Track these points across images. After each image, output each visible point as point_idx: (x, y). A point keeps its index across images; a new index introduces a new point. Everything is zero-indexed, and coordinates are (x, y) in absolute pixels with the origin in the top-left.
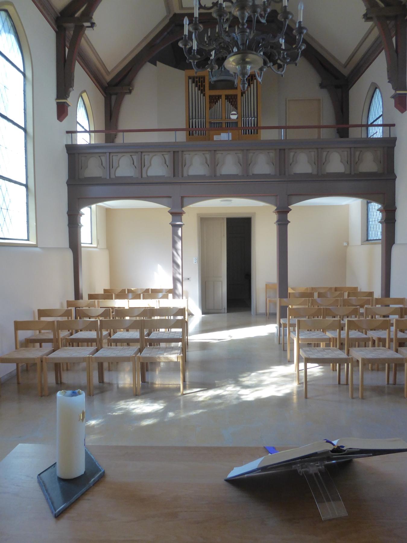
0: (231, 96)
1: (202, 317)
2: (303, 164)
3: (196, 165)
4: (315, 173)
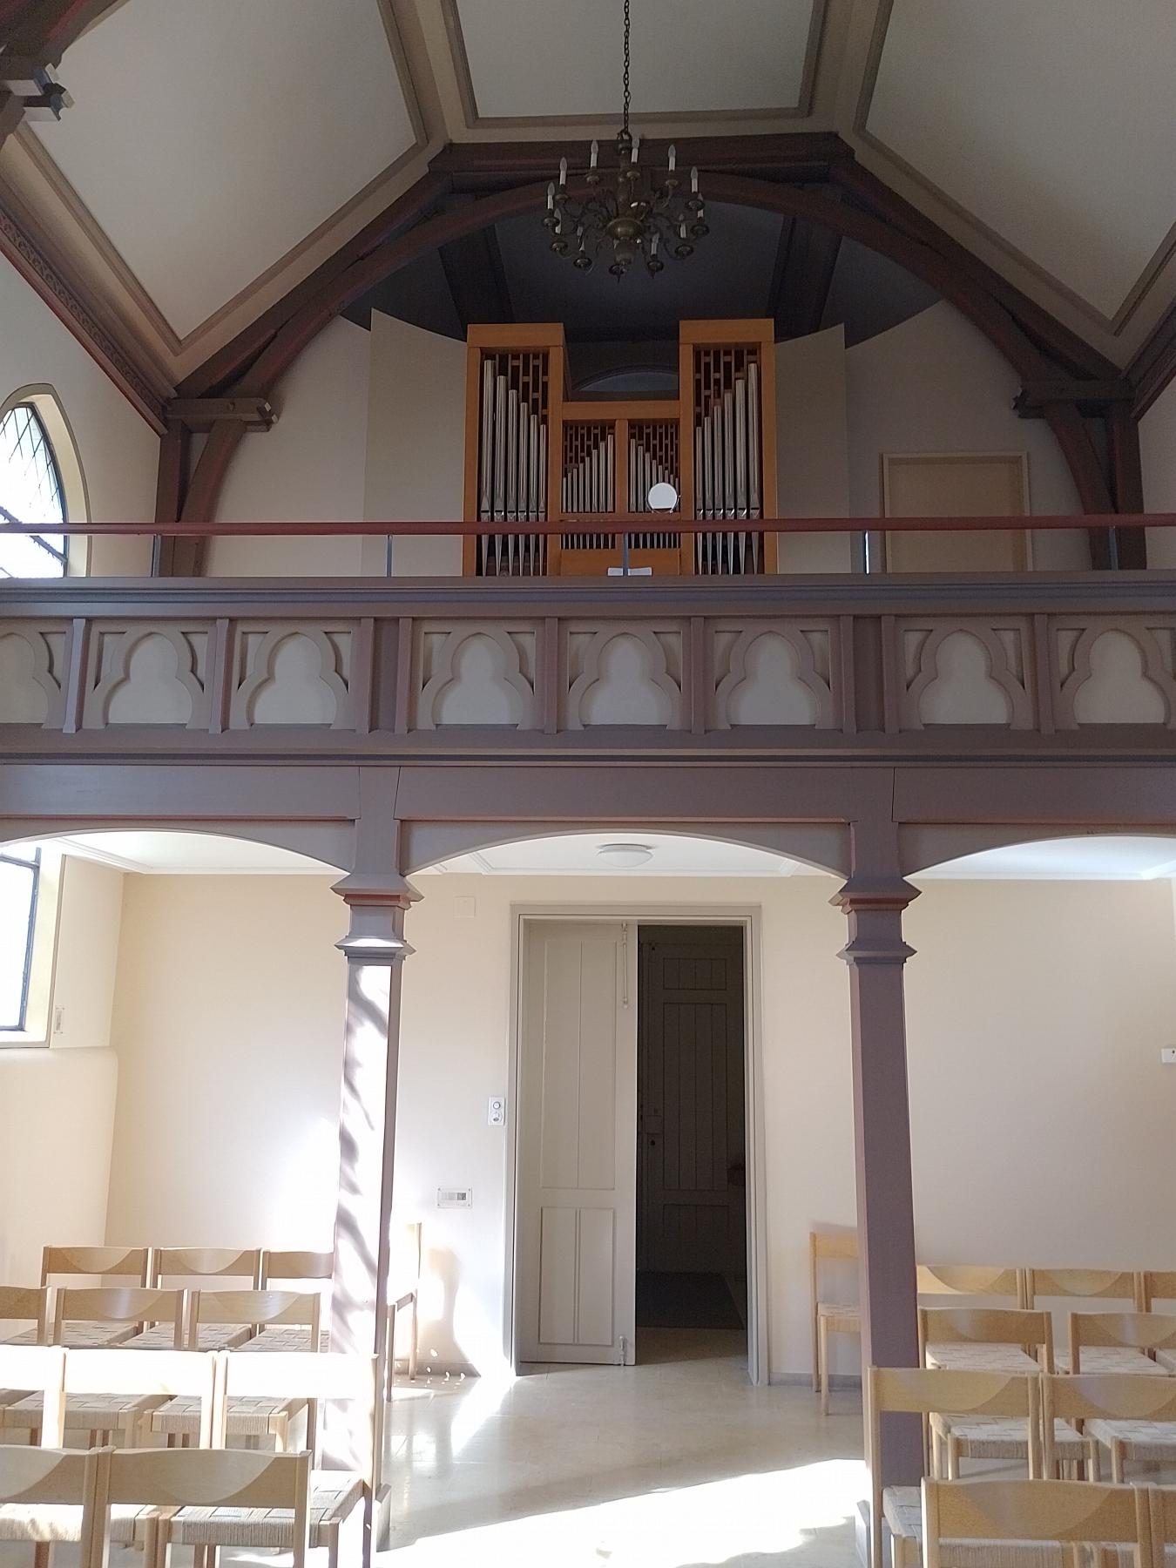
0: (655, 424)
1: (517, 1386)
2: (964, 685)
3: (478, 685)
4: (1025, 722)
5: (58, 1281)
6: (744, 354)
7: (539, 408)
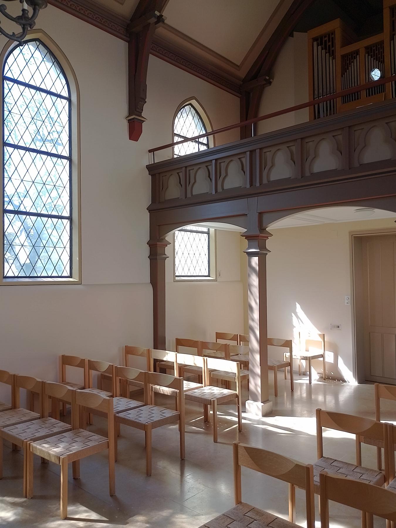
5: (220, 341)
7: (332, 54)
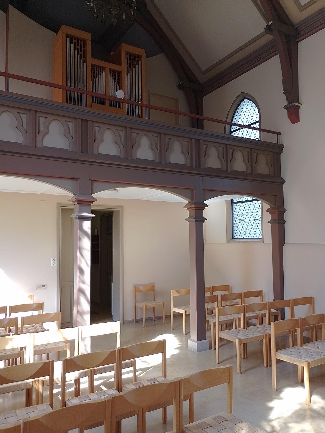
2: (108, 145)
6: (137, 58)
